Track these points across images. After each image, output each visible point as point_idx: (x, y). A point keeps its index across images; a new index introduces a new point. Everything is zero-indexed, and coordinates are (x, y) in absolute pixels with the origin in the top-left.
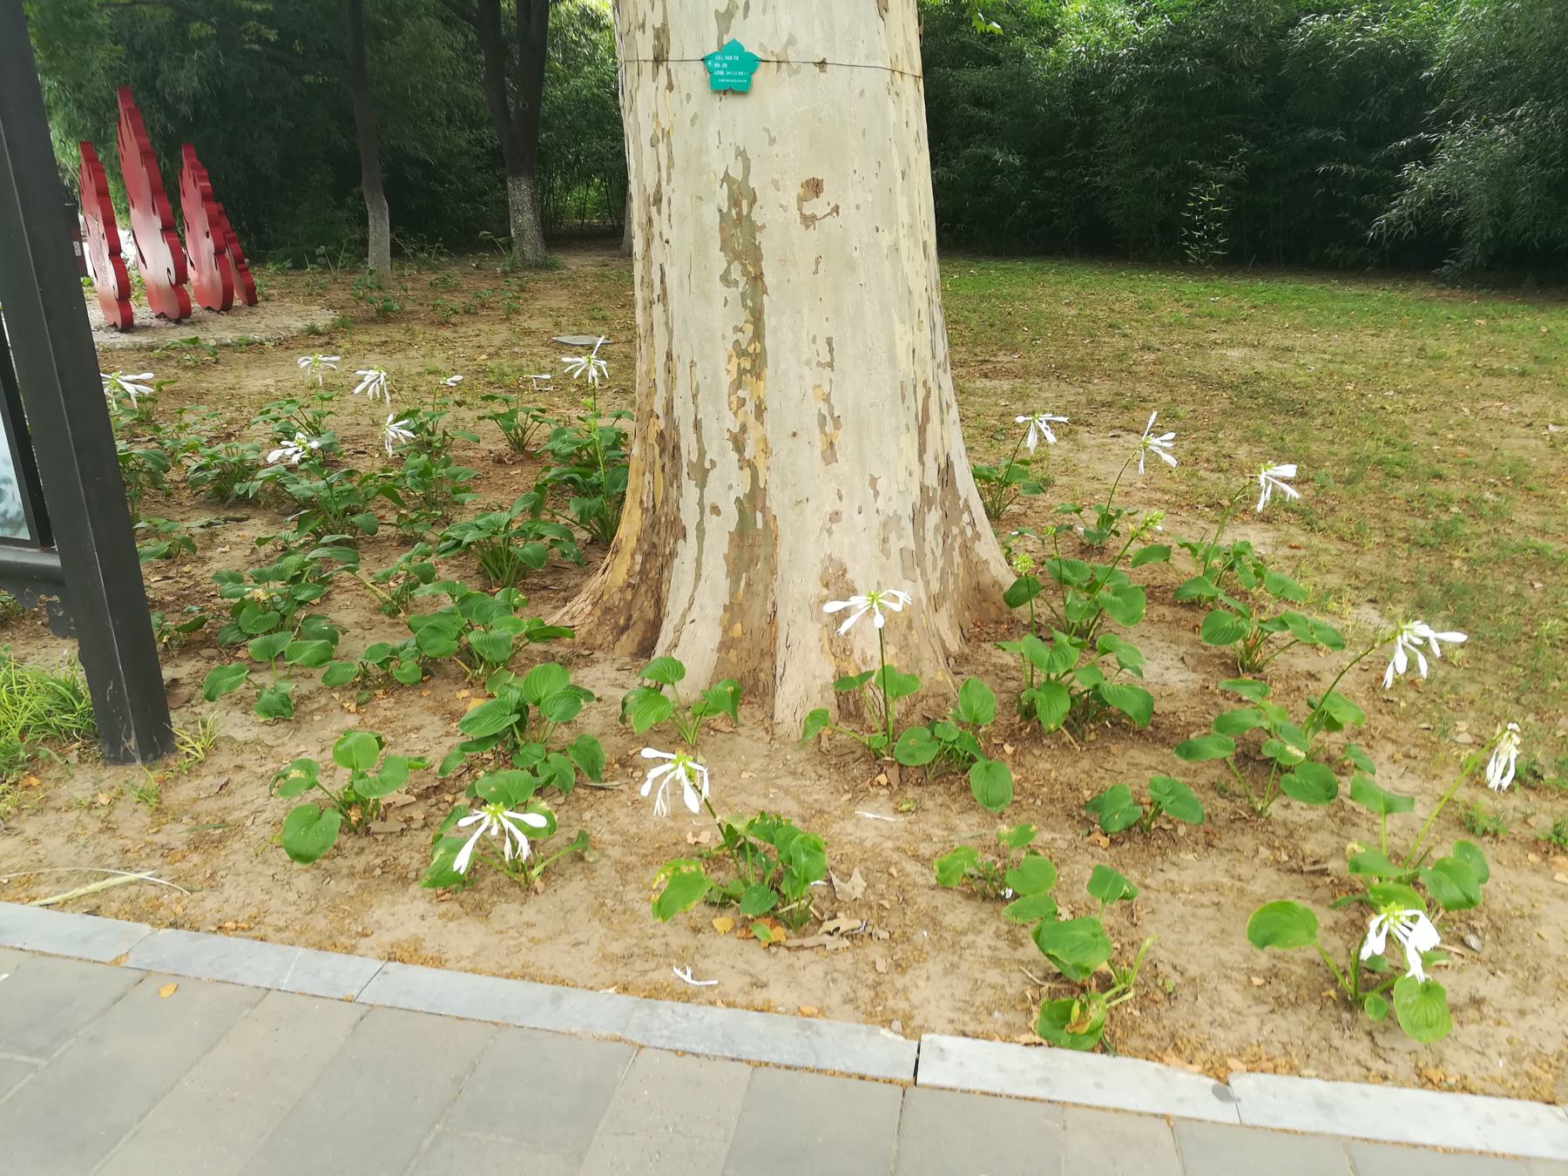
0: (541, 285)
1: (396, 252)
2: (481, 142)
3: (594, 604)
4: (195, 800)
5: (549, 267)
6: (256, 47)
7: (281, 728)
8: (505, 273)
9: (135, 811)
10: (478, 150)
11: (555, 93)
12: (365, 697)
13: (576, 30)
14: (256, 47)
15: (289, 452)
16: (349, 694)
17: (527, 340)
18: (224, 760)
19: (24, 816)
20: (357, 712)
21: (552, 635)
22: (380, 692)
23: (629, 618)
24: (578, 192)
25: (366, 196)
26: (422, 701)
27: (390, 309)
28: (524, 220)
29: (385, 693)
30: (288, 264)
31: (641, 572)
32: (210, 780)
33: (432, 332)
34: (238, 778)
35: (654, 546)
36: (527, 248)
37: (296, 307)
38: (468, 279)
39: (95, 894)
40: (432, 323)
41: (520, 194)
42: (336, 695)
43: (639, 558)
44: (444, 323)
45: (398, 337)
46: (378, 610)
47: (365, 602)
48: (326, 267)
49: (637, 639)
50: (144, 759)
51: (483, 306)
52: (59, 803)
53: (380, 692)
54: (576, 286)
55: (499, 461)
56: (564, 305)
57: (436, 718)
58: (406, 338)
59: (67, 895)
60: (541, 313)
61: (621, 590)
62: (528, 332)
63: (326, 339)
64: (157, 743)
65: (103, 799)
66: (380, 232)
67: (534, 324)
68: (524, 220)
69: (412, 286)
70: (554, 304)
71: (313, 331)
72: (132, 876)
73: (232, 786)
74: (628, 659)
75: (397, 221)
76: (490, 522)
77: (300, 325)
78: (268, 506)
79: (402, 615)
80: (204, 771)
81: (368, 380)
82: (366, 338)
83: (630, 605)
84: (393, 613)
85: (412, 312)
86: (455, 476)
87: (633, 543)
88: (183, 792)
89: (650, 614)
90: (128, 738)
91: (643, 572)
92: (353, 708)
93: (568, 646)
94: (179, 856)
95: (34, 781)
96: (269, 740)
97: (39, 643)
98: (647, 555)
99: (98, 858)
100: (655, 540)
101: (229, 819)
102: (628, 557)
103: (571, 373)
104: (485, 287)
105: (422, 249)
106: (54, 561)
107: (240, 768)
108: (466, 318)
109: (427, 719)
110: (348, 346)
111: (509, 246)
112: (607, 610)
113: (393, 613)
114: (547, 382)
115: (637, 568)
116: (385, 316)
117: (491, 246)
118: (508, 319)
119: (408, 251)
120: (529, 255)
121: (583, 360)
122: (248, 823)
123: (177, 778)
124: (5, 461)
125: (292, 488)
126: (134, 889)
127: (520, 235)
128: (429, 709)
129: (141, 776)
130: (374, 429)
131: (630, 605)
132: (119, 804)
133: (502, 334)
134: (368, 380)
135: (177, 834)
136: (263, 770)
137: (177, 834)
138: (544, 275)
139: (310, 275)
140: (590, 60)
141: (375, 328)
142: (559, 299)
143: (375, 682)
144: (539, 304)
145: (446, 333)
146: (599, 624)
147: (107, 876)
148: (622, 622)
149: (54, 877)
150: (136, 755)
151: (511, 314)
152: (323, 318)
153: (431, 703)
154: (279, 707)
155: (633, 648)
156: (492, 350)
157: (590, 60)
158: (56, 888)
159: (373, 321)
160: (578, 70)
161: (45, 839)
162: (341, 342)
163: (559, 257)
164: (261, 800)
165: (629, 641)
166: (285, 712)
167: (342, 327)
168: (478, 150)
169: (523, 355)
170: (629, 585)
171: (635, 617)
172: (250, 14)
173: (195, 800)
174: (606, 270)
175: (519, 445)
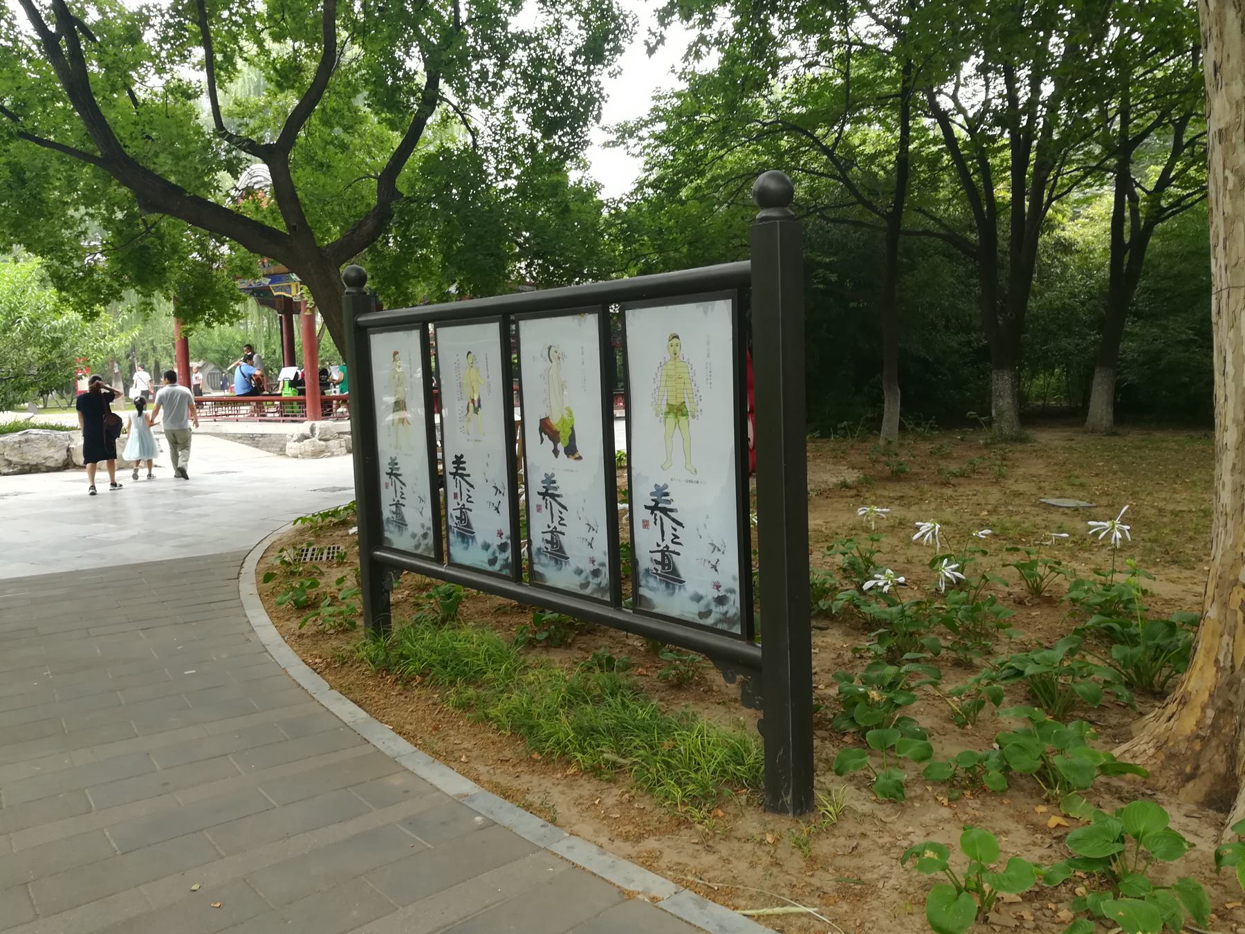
0: (1017, 455)
1: (902, 428)
2: (969, 343)
3: (1158, 748)
4: (836, 855)
5: (1022, 440)
6: (821, 286)
7: (889, 808)
8: (986, 445)
9: (792, 854)
10: (965, 350)
11: (1032, 304)
12: (956, 794)
13: (1049, 256)
14: (821, 286)
15: (881, 584)
16: (940, 789)
17: (1017, 501)
18: (849, 826)
19: (717, 839)
20: (949, 806)
21: (1116, 768)
22: (968, 793)
23: (1197, 768)
24: (1040, 381)
25: (885, 386)
26: (1003, 808)
27: (903, 472)
28: (1004, 404)
29: (972, 794)
30: (817, 434)
31: (1213, 726)
32: (842, 841)
33: (938, 490)
34: (865, 843)
35: (1231, 704)
36: (1005, 426)
37: (829, 467)
38: (959, 451)
39: (778, 916)
40: (936, 483)
41: (1002, 383)
42: (930, 788)
43: (1211, 713)
44: (945, 484)
45: (911, 493)
46: (950, 720)
47: (936, 711)
48: (844, 436)
49: (1204, 790)
50: (794, 813)
51: (974, 471)
52: (739, 834)
53: (968, 793)
54: (1049, 457)
55: (1020, 602)
56: (1043, 472)
57: (1020, 827)
58: (916, 494)
59: (761, 911)
60: (1025, 478)
61: (1188, 739)
62: (1017, 494)
63: (853, 492)
64: (804, 803)
65: (769, 839)
66: (892, 411)
67: (1021, 487)
68: (1004, 404)
69: (917, 452)
70: (1033, 471)
71: (845, 485)
72: (802, 909)
73: (860, 850)
74: (1194, 807)
75: (908, 407)
76: (1044, 658)
77: (834, 480)
78: (844, 621)
79: (969, 727)
80: (836, 832)
81: (923, 530)
82: (886, 493)
83: (1198, 756)
84: (962, 725)
85: (917, 474)
86: (997, 614)
87: (1205, 697)
88: (824, 847)
89: (1222, 768)
90: (787, 794)
91: (1214, 725)
92: (946, 802)
93: (1129, 782)
94: (832, 901)
95: (720, 813)
96: (881, 815)
97: (704, 705)
98: (1220, 712)
99: (775, 886)
100: (1232, 697)
101: (864, 878)
102: (1198, 711)
103: (1096, 534)
104: (973, 455)
105: (918, 425)
106: (755, 651)
107: (864, 835)
108: (961, 480)
109: (1010, 825)
110: (873, 498)
111: (989, 423)
112: (1172, 756)
113: (962, 725)
114: (1066, 539)
115: (1209, 721)
116: (898, 476)
117: (974, 424)
118: (997, 482)
119: (910, 427)
120: (1006, 431)
121: (1108, 524)
122: (880, 886)
123: (818, 833)
124: (734, 578)
125: (864, 609)
126: (805, 920)
127: (1000, 414)
128: (1012, 816)
129: (784, 824)
130: (909, 566)
131: (1198, 756)
132: (780, 845)
133: (994, 495)
134: (923, 530)
135: (826, 880)
136: (881, 841)
137: (826, 880)
138: (1019, 447)
139: (831, 443)
140: (1061, 277)
141: (890, 485)
142: (1038, 467)
143: (967, 783)
144: (1021, 471)
145: (948, 492)
146: (1163, 767)
147: (784, 905)
148: (1188, 769)
149: (747, 894)
150: (790, 809)
151: (999, 478)
152: (852, 476)
153: (1012, 811)
154: (893, 791)
155: (1200, 797)
156: (989, 507)
157: (1061, 277)
158: (750, 903)
159: (888, 479)
160: (1050, 286)
161: (734, 862)
162: (867, 495)
163: (1030, 432)
164: (886, 868)
165: (1197, 789)
166: (895, 796)
167: (866, 482)
168: (965, 350)
169: (1017, 513)
170: (1198, 737)
171: (1204, 767)
172: (820, 265)
173: (836, 855)
174: (1073, 444)
175: (1036, 591)
